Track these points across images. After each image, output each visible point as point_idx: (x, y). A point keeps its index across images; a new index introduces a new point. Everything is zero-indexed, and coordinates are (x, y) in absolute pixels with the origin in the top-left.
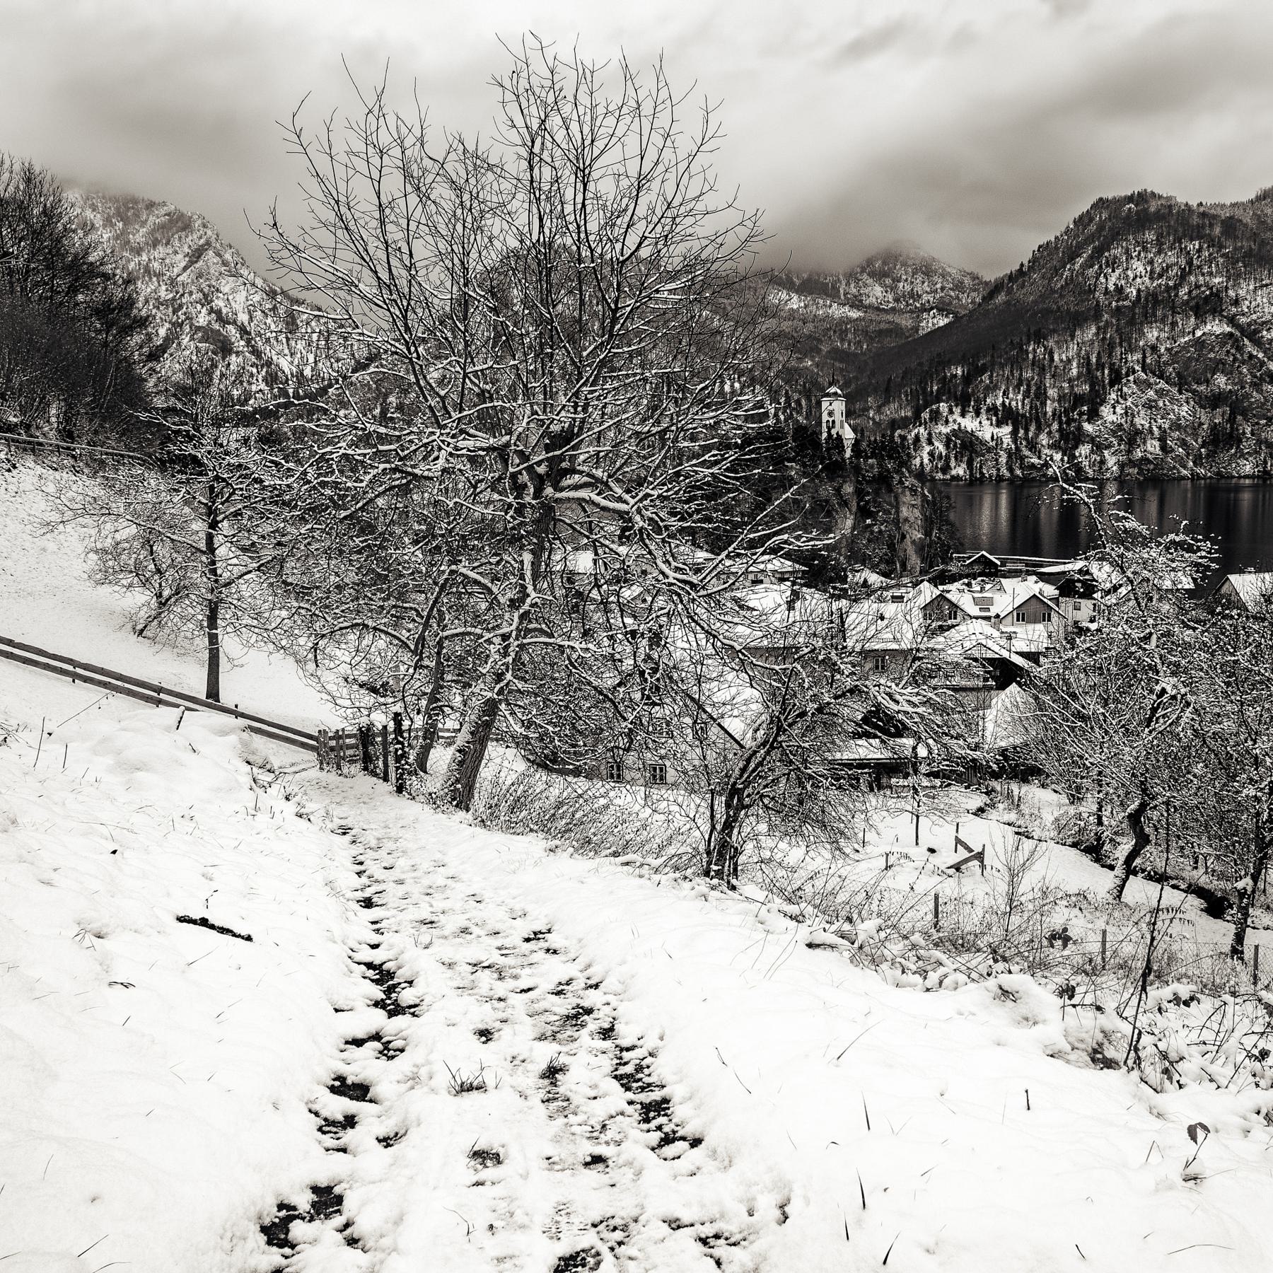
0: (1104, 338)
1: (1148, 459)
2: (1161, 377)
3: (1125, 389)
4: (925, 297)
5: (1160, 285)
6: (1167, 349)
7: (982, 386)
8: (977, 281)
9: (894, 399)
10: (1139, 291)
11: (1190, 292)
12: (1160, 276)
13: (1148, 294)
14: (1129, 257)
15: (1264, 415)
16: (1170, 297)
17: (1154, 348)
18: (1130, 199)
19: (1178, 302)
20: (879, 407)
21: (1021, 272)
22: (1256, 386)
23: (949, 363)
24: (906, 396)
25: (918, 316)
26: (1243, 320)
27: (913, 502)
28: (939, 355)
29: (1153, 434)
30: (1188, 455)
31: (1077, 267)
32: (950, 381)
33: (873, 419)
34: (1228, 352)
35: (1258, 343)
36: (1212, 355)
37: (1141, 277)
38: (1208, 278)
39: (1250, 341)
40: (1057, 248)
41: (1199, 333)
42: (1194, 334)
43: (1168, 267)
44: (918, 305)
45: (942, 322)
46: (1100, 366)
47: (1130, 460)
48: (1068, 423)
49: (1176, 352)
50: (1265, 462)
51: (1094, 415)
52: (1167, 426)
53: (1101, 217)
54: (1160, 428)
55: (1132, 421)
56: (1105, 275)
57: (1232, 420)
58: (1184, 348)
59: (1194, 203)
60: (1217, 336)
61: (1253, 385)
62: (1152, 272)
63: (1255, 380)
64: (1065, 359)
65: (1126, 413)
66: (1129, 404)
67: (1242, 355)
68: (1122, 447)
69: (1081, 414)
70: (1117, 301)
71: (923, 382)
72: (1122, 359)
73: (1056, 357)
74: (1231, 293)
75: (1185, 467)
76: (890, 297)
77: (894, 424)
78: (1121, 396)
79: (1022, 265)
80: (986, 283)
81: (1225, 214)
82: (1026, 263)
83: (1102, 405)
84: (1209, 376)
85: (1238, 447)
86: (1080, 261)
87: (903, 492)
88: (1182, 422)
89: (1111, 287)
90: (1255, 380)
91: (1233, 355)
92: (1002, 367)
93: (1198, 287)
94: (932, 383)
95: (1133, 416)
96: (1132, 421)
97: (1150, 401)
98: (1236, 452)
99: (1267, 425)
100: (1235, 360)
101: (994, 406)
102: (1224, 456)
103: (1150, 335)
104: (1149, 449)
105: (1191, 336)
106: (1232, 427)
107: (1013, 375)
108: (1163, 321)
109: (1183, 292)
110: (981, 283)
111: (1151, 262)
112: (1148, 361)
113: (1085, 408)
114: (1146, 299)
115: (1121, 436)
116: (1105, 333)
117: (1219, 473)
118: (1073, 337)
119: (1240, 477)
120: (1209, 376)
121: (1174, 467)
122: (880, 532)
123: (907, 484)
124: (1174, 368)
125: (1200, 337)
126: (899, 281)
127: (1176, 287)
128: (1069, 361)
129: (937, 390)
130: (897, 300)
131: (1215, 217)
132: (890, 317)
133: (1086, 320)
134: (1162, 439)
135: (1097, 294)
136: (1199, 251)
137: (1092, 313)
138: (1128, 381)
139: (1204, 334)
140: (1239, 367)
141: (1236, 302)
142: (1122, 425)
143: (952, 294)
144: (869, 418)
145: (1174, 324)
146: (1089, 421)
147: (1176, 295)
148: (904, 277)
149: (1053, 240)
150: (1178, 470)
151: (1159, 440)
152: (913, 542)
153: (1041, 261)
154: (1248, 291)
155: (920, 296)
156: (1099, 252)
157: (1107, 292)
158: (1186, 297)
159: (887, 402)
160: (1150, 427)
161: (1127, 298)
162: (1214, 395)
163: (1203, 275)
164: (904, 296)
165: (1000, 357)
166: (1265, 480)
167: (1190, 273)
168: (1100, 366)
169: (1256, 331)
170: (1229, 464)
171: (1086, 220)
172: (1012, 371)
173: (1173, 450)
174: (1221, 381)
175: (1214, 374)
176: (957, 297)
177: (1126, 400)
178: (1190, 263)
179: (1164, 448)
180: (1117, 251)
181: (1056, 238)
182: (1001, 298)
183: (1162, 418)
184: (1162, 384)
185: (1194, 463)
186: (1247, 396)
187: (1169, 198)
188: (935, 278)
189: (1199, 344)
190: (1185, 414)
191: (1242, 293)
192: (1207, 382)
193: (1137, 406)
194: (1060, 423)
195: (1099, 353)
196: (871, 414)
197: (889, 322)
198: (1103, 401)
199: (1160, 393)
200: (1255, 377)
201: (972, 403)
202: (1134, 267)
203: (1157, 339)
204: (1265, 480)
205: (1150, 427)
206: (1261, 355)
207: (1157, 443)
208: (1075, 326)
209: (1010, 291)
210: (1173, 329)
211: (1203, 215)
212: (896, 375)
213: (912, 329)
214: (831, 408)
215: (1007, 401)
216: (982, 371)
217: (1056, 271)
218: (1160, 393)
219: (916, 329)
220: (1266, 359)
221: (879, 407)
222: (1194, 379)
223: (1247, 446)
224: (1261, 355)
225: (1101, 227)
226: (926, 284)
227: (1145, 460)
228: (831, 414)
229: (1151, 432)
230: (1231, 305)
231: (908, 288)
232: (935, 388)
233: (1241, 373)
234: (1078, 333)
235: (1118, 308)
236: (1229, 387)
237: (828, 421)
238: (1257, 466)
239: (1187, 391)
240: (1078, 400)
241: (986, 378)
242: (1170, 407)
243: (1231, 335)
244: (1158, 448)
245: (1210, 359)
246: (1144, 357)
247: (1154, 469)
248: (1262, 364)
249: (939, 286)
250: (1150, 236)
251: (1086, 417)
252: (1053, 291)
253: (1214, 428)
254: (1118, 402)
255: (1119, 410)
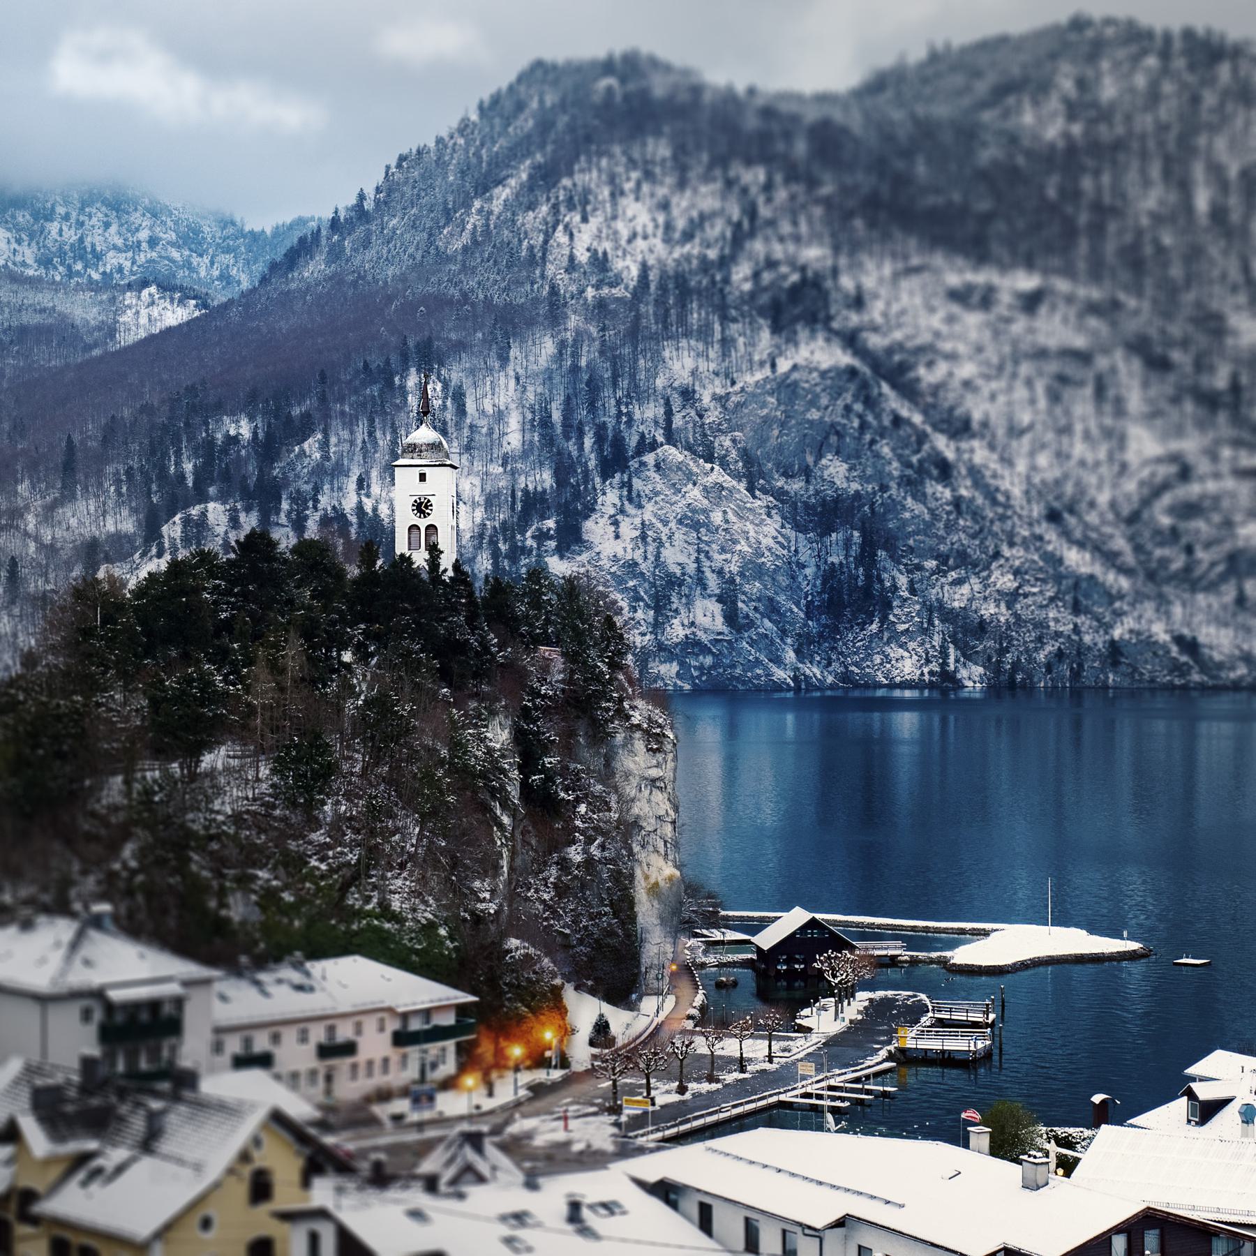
0: (575, 369)
1: (697, 643)
2: (709, 458)
3: (637, 484)
4: (112, 260)
5: (688, 258)
6: (716, 398)
7: (303, 468)
8: (230, 230)
9: (86, 489)
10: (645, 268)
11: (756, 275)
12: (688, 236)
13: (664, 276)
14: (617, 193)
15: (931, 549)
16: (713, 282)
17: (688, 395)
18: (608, 67)
19: (733, 296)
20: (51, 508)
21: (359, 212)
22: (912, 484)
23: (220, 408)
24: (118, 482)
25: (113, 300)
26: (875, 341)
27: (654, 773)
28: (191, 390)
29: (705, 587)
30: (784, 633)
31: (497, 206)
32: (225, 451)
33: (37, 539)
34: (848, 409)
35: (909, 391)
36: (814, 415)
37: (645, 237)
38: (791, 248)
39: (894, 386)
40: (440, 163)
41: (784, 366)
42: (773, 366)
43: (704, 218)
44: (96, 276)
45: (174, 315)
46: (573, 429)
47: (661, 647)
48: (513, 558)
49: (739, 405)
50: (944, 653)
51: (570, 539)
52: (734, 568)
53: (541, 102)
54: (720, 572)
55: (658, 556)
56: (566, 227)
57: (867, 556)
58: (752, 397)
59: (740, 87)
60: (824, 374)
61: (905, 482)
62: (669, 227)
63: (909, 472)
64: (489, 409)
65: (643, 537)
66: (648, 516)
67: (878, 417)
68: (640, 615)
69: (541, 536)
70: (597, 287)
71: (156, 452)
72: (620, 413)
73: (470, 406)
74: (847, 282)
75: (778, 661)
76: (28, 254)
77: (92, 551)
78: (630, 500)
79: (362, 197)
80: (255, 237)
81: (812, 115)
82: (370, 192)
83: (587, 517)
84: (810, 459)
85: (884, 619)
86: (502, 194)
87: (628, 741)
88: (767, 560)
89: (583, 257)
90: (909, 472)
91: (860, 416)
92: (350, 423)
93: (771, 264)
94: (178, 454)
95: (661, 544)
96: (658, 556)
97: (694, 511)
98: (881, 631)
99: (937, 571)
100: (864, 426)
101: (340, 516)
102: (855, 639)
103: (676, 366)
104: (701, 620)
105: (767, 371)
106: (868, 576)
107: (375, 443)
108: (704, 333)
109: (741, 274)
110: (241, 234)
111: (665, 206)
112: (678, 421)
113: (550, 523)
114: (662, 287)
115: (635, 589)
116: (576, 355)
117: (846, 677)
118: (504, 359)
119: (892, 686)
120: (810, 459)
121: (758, 662)
122: (589, 863)
123: (636, 718)
124: (734, 441)
125: (787, 375)
126: (49, 217)
127: (725, 262)
128: (500, 416)
129: (197, 472)
130: (45, 262)
131: (795, 119)
132: (44, 299)
133: (531, 323)
134: (727, 599)
135: (550, 269)
136: (768, 187)
137: (543, 309)
138: (643, 464)
139: (795, 367)
140: (873, 442)
141: (858, 301)
142: (636, 564)
143: (175, 254)
144: (26, 534)
145: (727, 343)
146: (561, 551)
147: (727, 280)
148: (61, 210)
149: (432, 144)
150: (766, 668)
151: (720, 599)
152: (654, 890)
153: (407, 190)
154: (881, 280)
155: (98, 257)
156: (545, 177)
157: (572, 265)
158: (747, 287)
159: (67, 496)
160: (699, 570)
161: (617, 281)
162: (824, 503)
163: (781, 239)
164: (62, 254)
165: (341, 399)
166: (944, 692)
167: (752, 234)
168: (573, 429)
169: (903, 368)
170: (869, 656)
171: (508, 105)
172: (371, 434)
173: (751, 624)
174: (835, 470)
175: (820, 456)
176: (188, 265)
177: (640, 507)
178: (751, 212)
179: (731, 617)
180: (588, 177)
181: (439, 141)
182: (315, 268)
183: (723, 550)
184: (718, 475)
185: (797, 652)
186: (894, 507)
187: (686, 72)
188: (136, 218)
189: (787, 388)
190: (771, 542)
191: (869, 282)
192: (807, 473)
193: (665, 523)
194: (496, 555)
195: (568, 400)
196: (31, 521)
197: (43, 311)
198: (590, 510)
199: (716, 492)
200: (908, 465)
201: (285, 505)
202: (630, 213)
203: (694, 373)
204: (944, 692)
205: (699, 570)
206: (917, 419)
207: (716, 608)
208: (506, 336)
209: (335, 254)
210: (725, 355)
211: (768, 113)
212: (89, 432)
213: (99, 328)
214: (423, 490)
215: (368, 505)
216: (303, 430)
217: (448, 214)
218: (716, 492)
219: (112, 332)
220: (929, 429)
221: (51, 508)
222: (778, 465)
223: (905, 614)
224: (917, 419)
225: (545, 125)
226: (113, 229)
227: (692, 645)
228: (422, 507)
229: (701, 582)
230: (849, 307)
231: (71, 236)
232: (188, 467)
233: (878, 456)
234: (514, 352)
235: (601, 304)
236: (855, 486)
237: (413, 528)
238: (928, 661)
239: (765, 491)
240: (533, 504)
241: (311, 446)
242: (737, 526)
243: (852, 372)
244: (720, 620)
245: (811, 422)
246: (669, 414)
247: (713, 667)
248: (922, 438)
249: (144, 235)
250: (661, 149)
251: (552, 544)
252: (443, 258)
253: (830, 575)
254: (622, 511)
255: (628, 530)
